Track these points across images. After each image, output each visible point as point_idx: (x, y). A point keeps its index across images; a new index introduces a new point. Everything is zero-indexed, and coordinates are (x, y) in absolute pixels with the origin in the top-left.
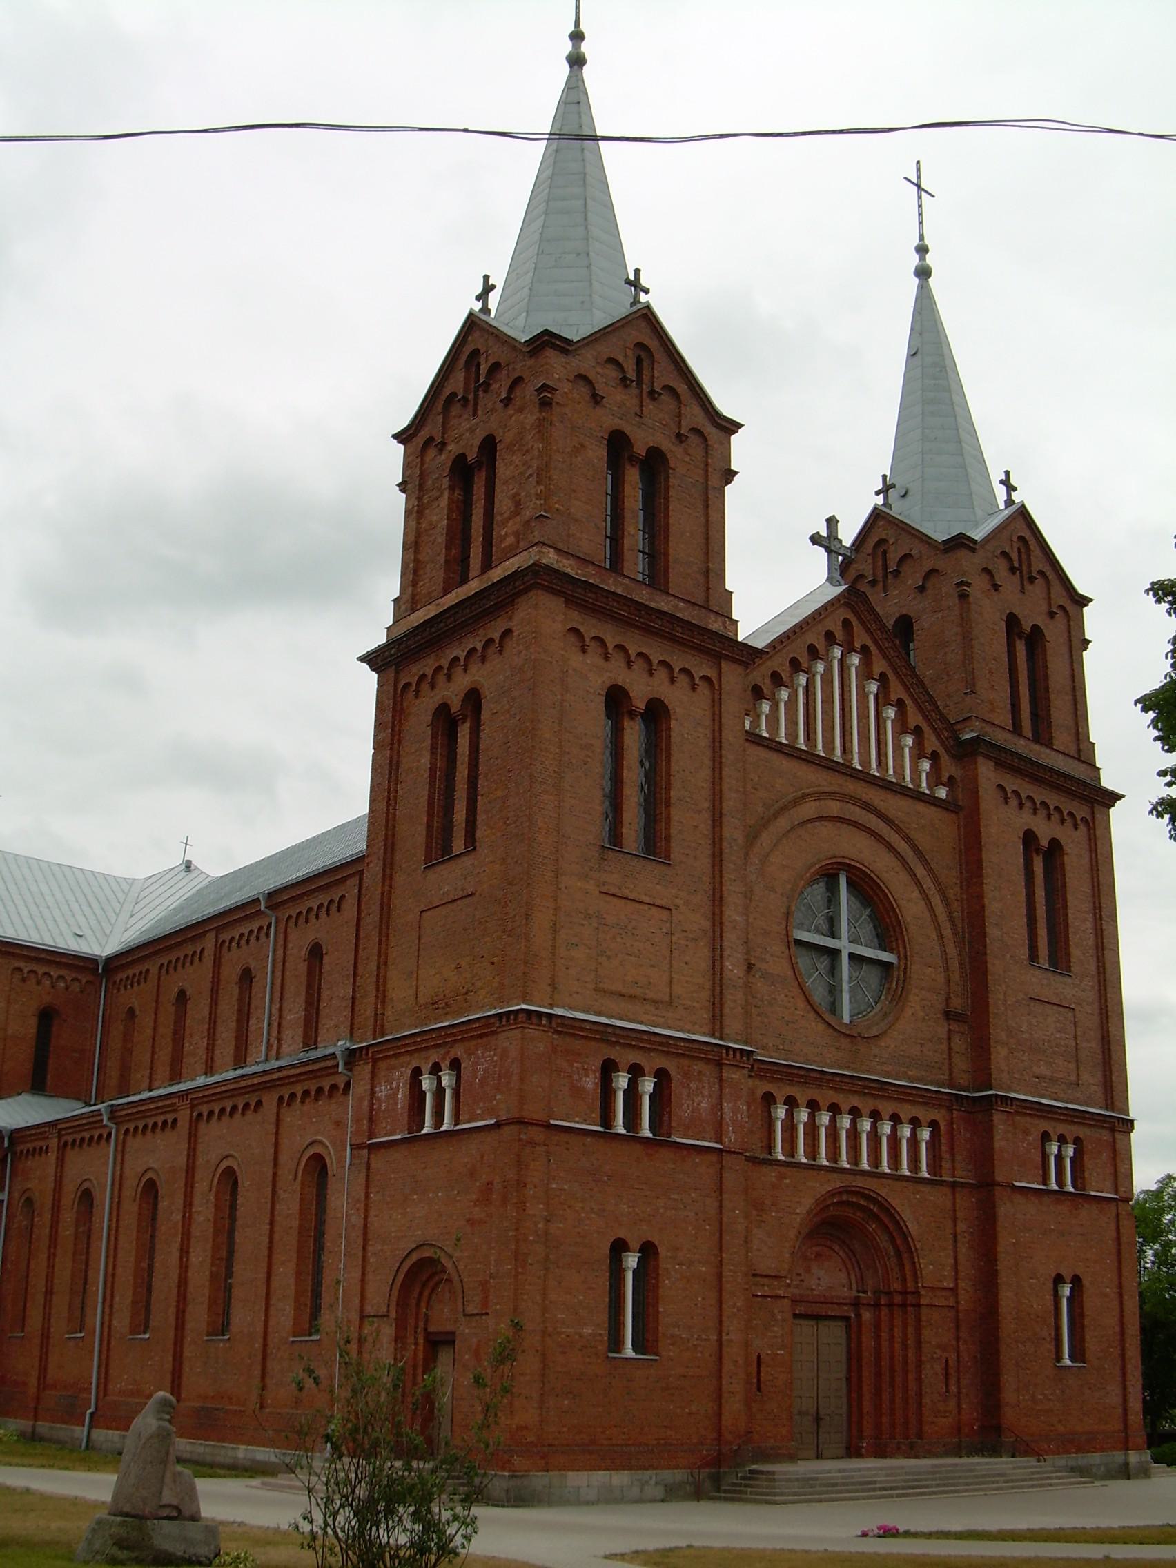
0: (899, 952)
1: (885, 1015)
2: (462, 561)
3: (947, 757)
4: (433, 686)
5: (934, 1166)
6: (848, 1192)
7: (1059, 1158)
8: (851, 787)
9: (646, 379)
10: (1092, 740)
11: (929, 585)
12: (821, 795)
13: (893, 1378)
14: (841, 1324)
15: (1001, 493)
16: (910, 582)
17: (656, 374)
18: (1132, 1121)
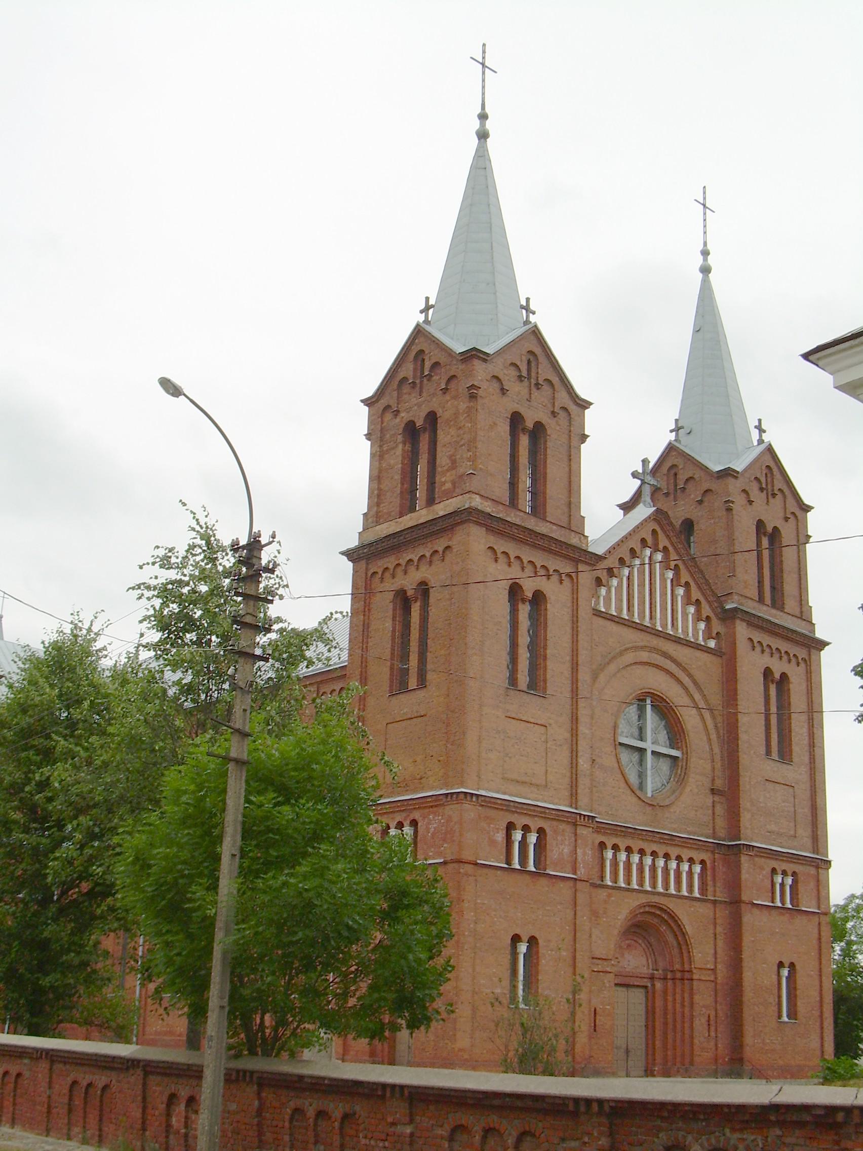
0: (682, 750)
1: (674, 791)
2: (411, 492)
3: (716, 620)
4: (393, 577)
5: (703, 889)
6: (649, 906)
7: (782, 885)
8: (655, 642)
9: (533, 374)
10: (810, 604)
11: (706, 499)
12: (636, 648)
13: (675, 1026)
14: (642, 990)
15: (755, 435)
16: (692, 496)
17: (540, 372)
18: (830, 862)
